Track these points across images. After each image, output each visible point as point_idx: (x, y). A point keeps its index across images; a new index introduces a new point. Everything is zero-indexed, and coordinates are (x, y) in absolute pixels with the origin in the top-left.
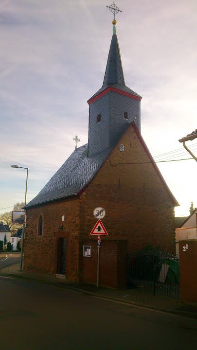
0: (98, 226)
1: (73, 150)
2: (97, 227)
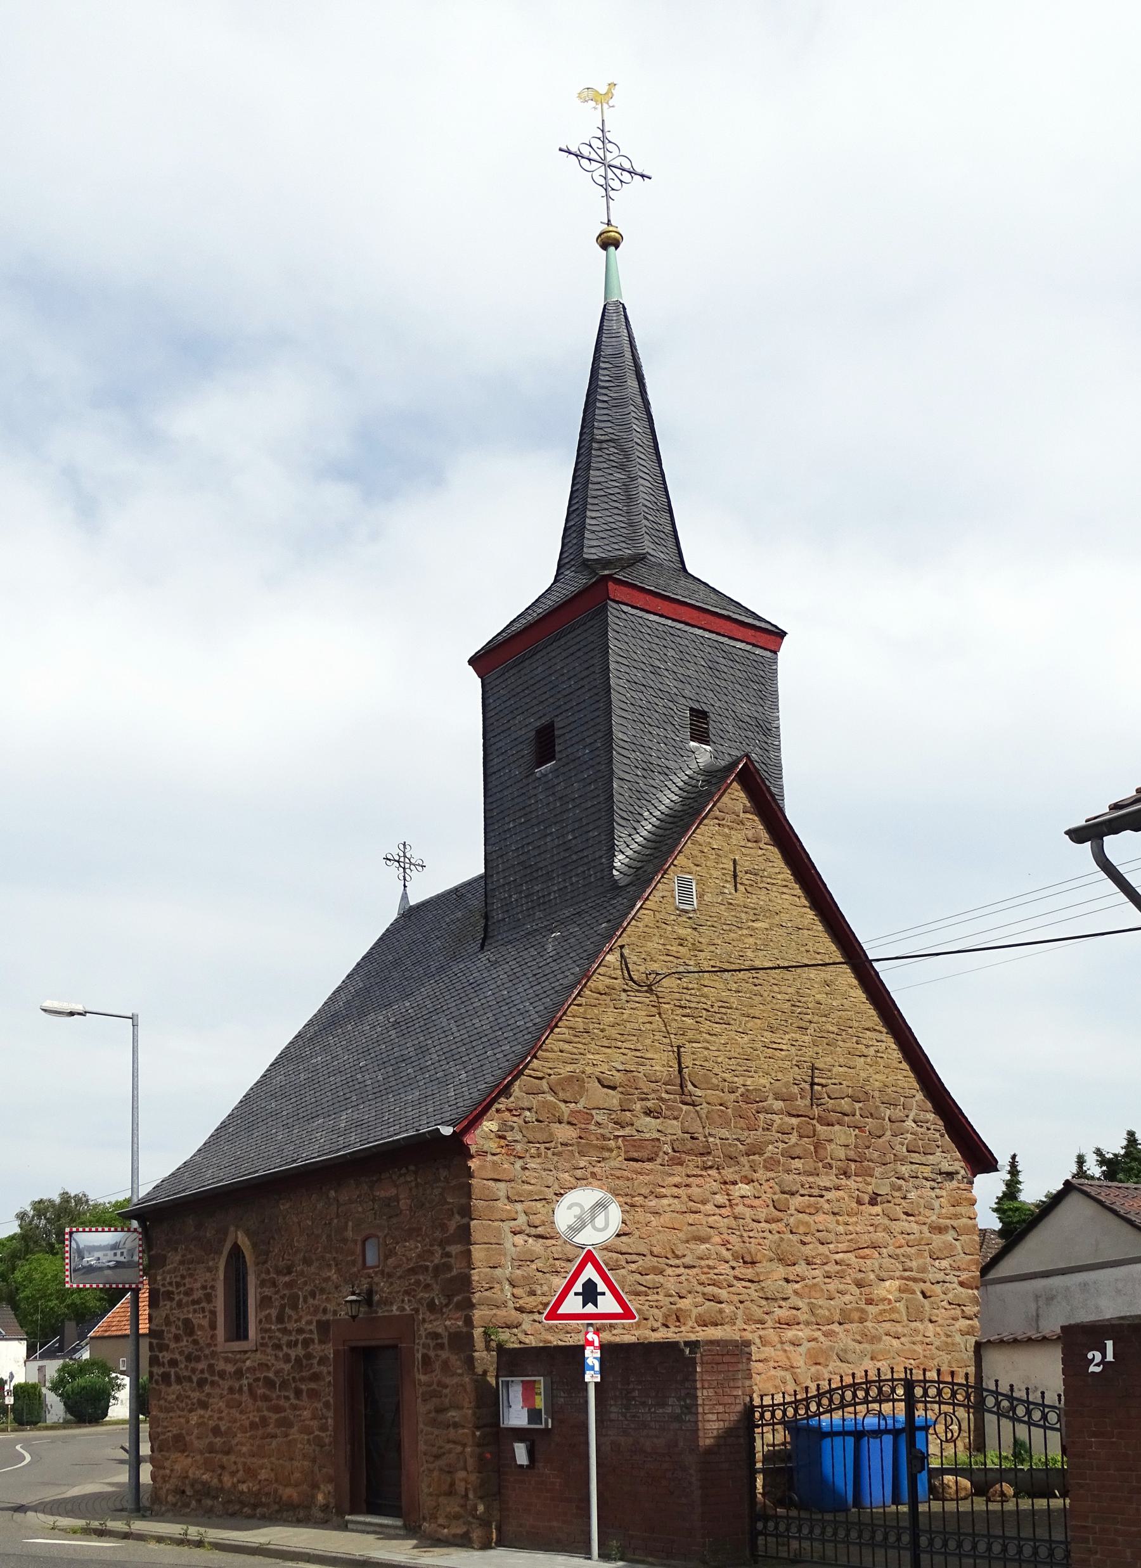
0: (582, 1279)
1: (391, 915)
2: (578, 1287)
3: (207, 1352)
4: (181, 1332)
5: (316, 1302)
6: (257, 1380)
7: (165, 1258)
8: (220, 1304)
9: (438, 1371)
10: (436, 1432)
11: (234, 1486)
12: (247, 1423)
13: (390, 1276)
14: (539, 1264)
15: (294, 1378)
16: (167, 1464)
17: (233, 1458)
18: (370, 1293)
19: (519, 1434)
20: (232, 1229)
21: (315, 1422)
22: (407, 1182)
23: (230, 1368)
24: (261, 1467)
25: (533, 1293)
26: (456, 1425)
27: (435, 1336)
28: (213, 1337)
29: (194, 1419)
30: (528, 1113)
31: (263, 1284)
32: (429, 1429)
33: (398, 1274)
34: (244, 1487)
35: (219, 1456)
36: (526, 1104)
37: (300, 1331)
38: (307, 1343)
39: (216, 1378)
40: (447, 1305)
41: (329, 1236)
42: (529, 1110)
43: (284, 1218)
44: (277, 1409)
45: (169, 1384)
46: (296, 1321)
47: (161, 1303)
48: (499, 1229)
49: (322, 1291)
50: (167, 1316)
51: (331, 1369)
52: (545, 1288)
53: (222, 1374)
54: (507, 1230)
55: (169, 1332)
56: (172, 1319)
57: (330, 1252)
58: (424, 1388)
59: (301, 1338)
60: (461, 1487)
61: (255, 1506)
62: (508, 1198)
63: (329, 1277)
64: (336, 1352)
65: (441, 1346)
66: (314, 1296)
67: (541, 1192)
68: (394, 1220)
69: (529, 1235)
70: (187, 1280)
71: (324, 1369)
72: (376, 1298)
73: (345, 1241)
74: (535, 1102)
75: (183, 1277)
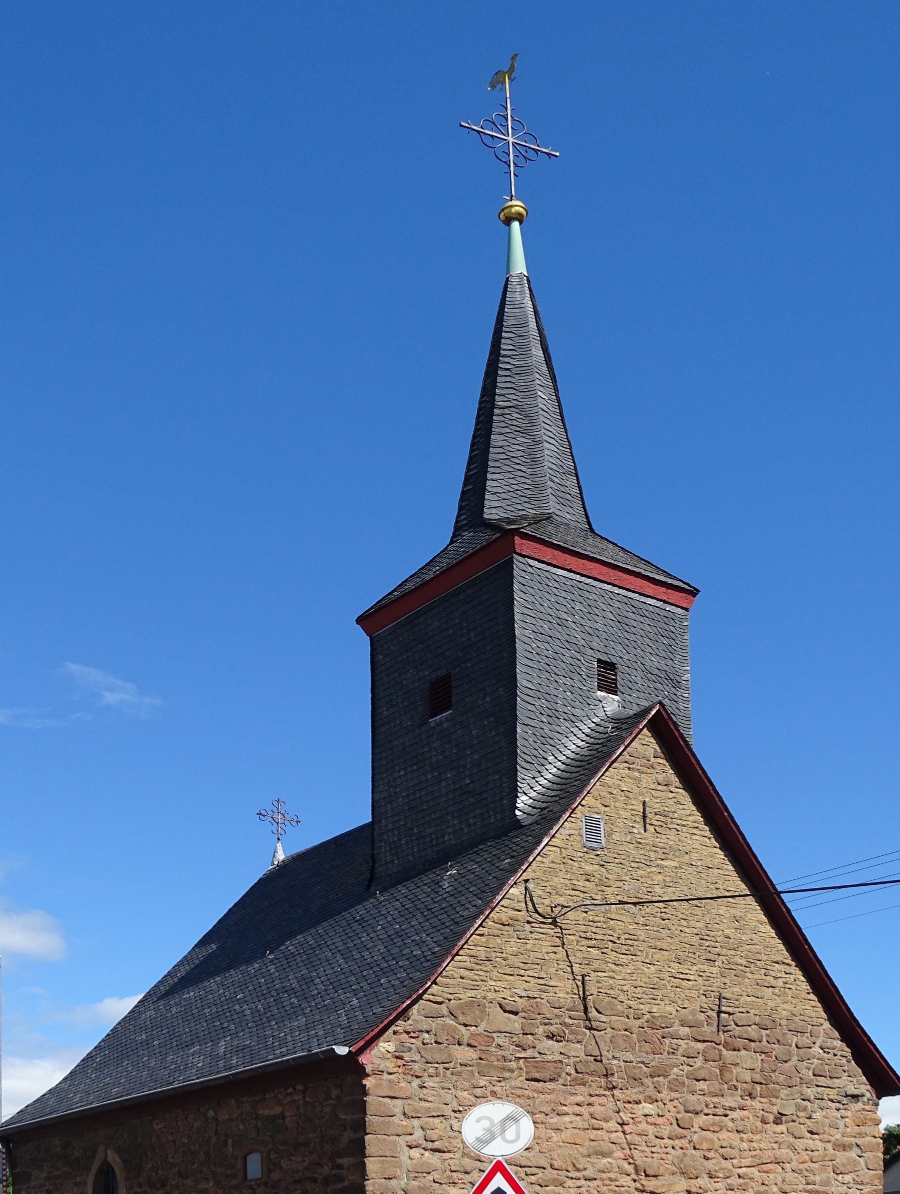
20: (101, 1148)
22: (294, 1101)
30: (426, 1035)
42: (428, 1032)
48: (395, 1144)
54: (404, 1144)
69: (425, 1149)
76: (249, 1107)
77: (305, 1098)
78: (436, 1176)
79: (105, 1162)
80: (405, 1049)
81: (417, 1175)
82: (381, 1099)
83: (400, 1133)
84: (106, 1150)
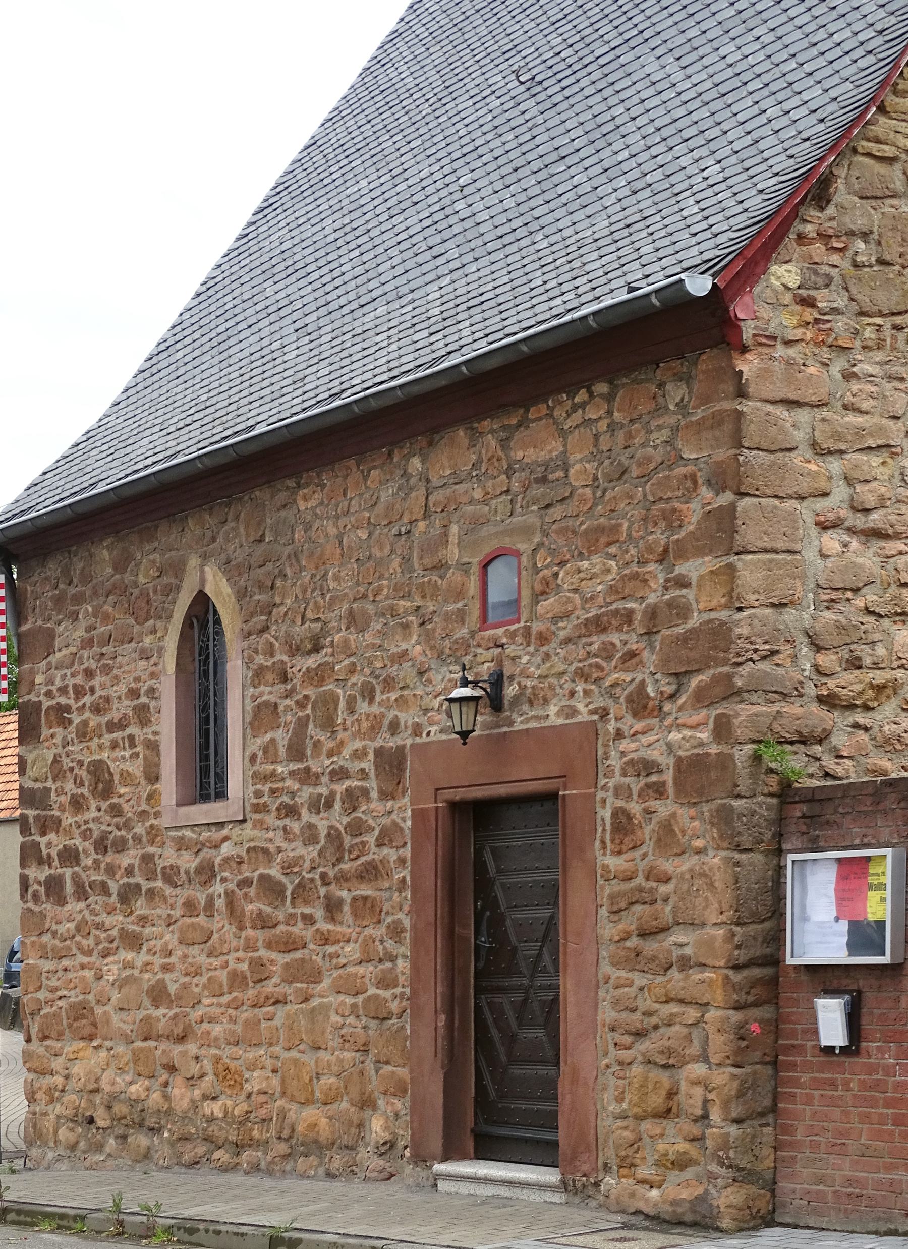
3: (139, 829)
4: (85, 791)
5: (375, 709)
6: (246, 883)
7: (51, 635)
8: (166, 726)
9: (648, 847)
10: (640, 980)
11: (195, 1106)
12: (223, 976)
13: (543, 639)
14: (870, 597)
15: (323, 876)
16: (57, 1064)
17: (192, 1048)
18: (498, 681)
19: (826, 978)
20: (194, 562)
21: (376, 964)
22: (587, 422)
23: (188, 862)
24: (252, 1067)
25: (855, 664)
26: (685, 964)
27: (648, 767)
28: (151, 797)
29: (112, 969)
30: (861, 245)
31: (259, 675)
32: (623, 973)
33: (562, 634)
34: (216, 1108)
35: (164, 1045)
36: (859, 223)
37: (340, 774)
38: (352, 799)
39: (159, 884)
40: (672, 697)
41: (406, 560)
42: (865, 235)
43: (308, 527)
44: (289, 945)
45: (61, 901)
46: (330, 754)
47: (45, 732)
48: (793, 518)
49: (389, 683)
50: (56, 761)
51: (407, 852)
52: (881, 651)
53: (170, 876)
54: (809, 519)
55: (60, 792)
56: (67, 763)
57: (407, 596)
58: (616, 887)
59: (339, 788)
60: (692, 1099)
61: (238, 1147)
62: (814, 445)
63: (405, 653)
64: (418, 815)
65: (659, 790)
66: (369, 694)
67: (881, 429)
68: (557, 512)
69: (851, 531)
70: (97, 681)
71: (391, 854)
72: (510, 691)
73: (441, 567)
74: (876, 217)
75: (89, 674)
76: (493, 443)
77: (610, 413)
78: (870, 597)
79: (202, 600)
80: (820, 281)
81: (834, 595)
82: (770, 408)
83: (803, 491)
84: (202, 566)
